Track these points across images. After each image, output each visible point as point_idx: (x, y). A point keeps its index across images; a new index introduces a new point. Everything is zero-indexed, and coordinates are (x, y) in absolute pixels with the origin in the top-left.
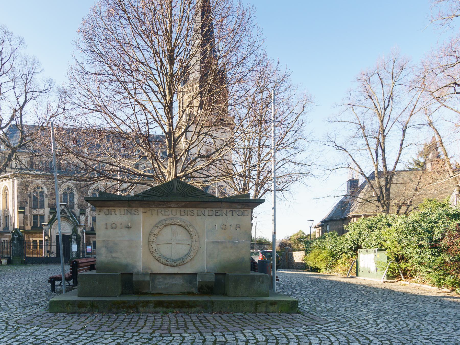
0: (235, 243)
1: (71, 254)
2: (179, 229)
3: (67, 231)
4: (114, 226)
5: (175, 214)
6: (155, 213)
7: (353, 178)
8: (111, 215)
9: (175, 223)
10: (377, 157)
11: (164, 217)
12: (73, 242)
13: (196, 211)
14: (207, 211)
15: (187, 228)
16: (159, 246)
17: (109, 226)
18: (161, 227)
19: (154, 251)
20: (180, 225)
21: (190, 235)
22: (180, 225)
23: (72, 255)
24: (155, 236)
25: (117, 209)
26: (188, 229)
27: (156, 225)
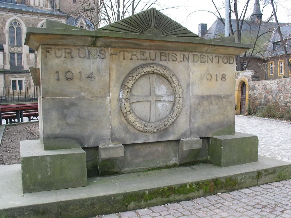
4: (69, 75)
7: (181, 199)
9: (155, 71)
10: (171, 31)
15: (169, 78)
16: (134, 105)
17: (62, 76)
18: (137, 77)
19: (128, 113)
27: (131, 74)
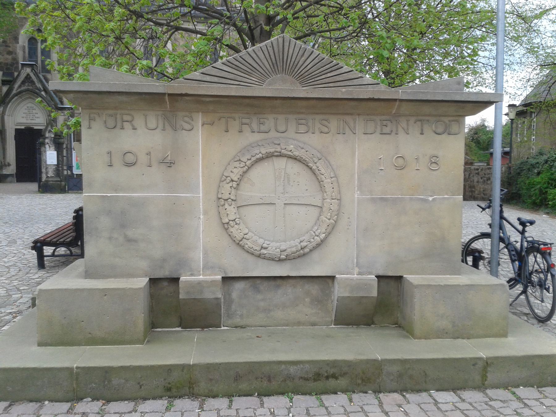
0: (426, 201)
1: (44, 170)
2: (294, 168)
3: (37, 121)
4: (130, 158)
5: (282, 129)
6: (235, 125)
8: (122, 128)
11: (257, 137)
12: (47, 146)
13: (334, 123)
14: (360, 124)
18: (248, 163)
20: (295, 158)
21: (320, 182)
22: (295, 158)
23: (47, 173)
24: (235, 184)
25: (139, 121)
26: (314, 167)
